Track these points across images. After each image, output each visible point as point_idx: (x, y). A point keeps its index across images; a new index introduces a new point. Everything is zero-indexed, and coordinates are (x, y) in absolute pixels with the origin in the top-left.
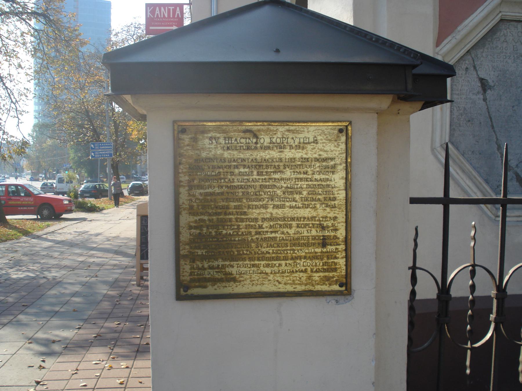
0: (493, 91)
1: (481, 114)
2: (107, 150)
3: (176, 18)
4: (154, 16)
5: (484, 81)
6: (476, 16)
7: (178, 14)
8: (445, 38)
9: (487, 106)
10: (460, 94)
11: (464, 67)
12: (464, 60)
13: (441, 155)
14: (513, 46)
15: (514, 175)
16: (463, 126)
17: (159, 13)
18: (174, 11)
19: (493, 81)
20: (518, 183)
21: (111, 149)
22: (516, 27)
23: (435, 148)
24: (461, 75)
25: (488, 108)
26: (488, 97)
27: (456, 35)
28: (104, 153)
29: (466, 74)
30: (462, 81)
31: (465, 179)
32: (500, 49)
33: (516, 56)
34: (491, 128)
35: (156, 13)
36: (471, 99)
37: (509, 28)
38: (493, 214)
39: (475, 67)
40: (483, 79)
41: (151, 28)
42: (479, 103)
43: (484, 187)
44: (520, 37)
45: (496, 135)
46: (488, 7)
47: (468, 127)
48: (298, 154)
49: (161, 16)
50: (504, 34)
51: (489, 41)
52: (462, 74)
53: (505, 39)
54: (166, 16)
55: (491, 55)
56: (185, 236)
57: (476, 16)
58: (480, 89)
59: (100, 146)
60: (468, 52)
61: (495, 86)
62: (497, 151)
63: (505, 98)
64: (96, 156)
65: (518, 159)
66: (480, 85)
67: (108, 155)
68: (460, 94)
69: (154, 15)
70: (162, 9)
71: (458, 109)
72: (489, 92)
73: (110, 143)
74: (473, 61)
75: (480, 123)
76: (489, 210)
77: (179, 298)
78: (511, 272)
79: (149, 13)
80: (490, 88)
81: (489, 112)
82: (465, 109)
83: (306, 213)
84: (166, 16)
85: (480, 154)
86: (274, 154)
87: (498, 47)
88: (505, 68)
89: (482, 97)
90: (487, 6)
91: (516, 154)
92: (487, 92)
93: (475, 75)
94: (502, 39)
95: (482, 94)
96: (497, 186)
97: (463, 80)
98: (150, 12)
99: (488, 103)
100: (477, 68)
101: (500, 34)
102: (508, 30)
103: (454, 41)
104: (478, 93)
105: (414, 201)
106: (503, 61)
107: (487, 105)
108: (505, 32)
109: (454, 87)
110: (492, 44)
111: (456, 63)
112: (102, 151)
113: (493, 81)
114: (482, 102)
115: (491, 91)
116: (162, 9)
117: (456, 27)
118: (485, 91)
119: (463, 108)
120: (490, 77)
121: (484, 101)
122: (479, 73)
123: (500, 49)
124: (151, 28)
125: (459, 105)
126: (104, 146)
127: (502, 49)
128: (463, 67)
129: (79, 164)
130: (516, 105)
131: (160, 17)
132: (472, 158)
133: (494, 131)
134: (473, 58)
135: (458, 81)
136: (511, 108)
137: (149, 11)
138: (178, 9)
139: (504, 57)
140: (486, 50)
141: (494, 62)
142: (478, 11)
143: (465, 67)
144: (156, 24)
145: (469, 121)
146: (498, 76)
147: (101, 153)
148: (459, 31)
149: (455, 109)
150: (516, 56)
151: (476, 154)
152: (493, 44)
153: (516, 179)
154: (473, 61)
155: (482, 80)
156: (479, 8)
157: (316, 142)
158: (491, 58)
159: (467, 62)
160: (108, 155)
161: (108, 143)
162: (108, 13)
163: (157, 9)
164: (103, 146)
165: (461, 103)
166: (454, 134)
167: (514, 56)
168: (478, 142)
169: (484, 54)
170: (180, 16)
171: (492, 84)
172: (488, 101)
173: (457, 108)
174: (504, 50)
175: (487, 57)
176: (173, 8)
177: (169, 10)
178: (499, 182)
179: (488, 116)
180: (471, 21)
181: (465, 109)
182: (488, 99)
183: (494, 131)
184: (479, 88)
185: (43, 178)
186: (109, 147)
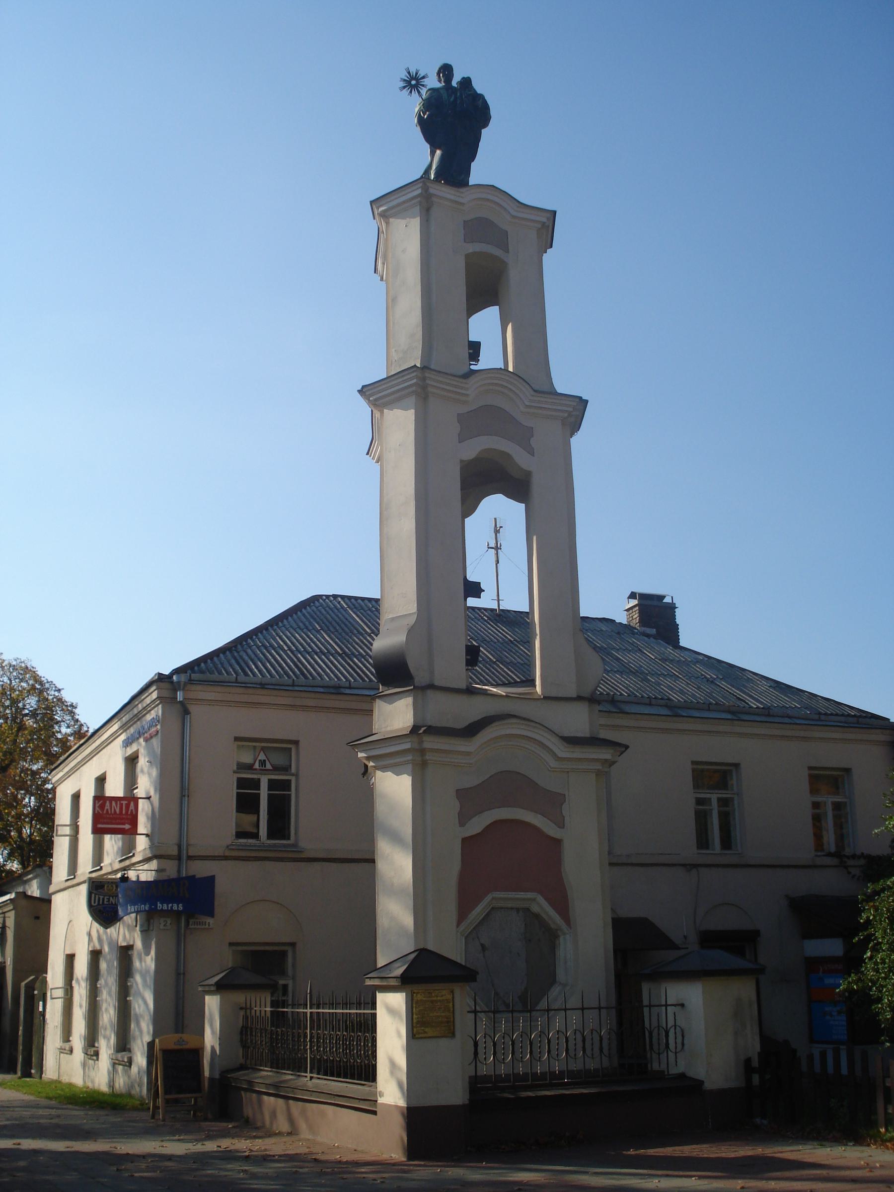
3: (129, 815)
7: (132, 810)
17: (109, 808)
18: (128, 806)
35: (106, 808)
48: (441, 999)
49: (111, 812)
56: (415, 1021)
60: (474, 928)
70: (114, 803)
78: (497, 1036)
83: (443, 1014)
84: (118, 811)
86: (435, 998)
98: (98, 807)
116: (114, 803)
124: (100, 826)
129: (417, 1000)
131: (110, 813)
137: (97, 805)
157: (445, 995)
170: (134, 813)
176: (126, 802)
185: (889, 979)
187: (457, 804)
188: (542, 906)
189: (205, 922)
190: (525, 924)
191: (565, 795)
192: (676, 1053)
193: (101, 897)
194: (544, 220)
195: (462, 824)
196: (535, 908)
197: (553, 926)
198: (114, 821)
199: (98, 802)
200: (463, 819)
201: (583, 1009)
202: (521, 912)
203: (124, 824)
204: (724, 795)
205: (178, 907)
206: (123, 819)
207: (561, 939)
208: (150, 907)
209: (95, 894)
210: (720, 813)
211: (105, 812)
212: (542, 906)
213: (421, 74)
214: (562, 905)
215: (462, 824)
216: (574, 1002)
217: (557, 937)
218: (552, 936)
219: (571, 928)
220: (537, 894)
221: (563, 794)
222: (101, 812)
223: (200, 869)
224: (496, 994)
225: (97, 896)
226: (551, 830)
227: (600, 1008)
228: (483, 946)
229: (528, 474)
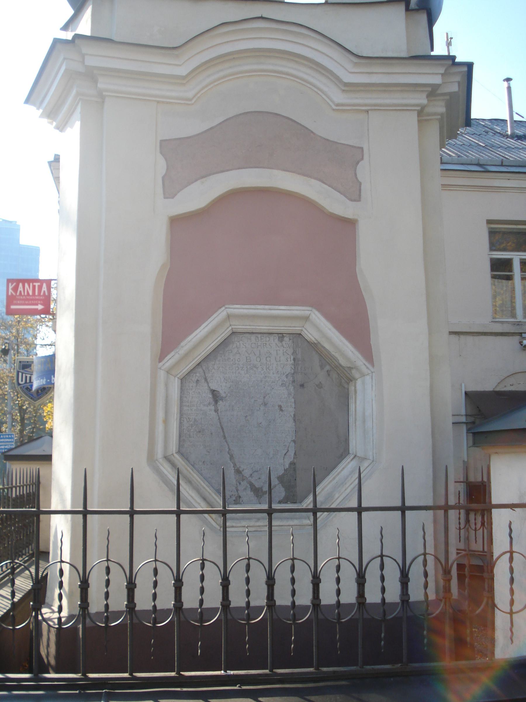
0: (224, 402)
1: (212, 425)
2: (7, 443)
5: (216, 392)
6: (200, 331)
8: (169, 353)
9: (219, 417)
10: (190, 406)
11: (194, 379)
12: (195, 373)
13: (163, 467)
14: (246, 357)
15: (248, 485)
16: (193, 437)
17: (22, 290)
18: (40, 288)
19: (225, 392)
20: (252, 493)
21: (13, 442)
22: (249, 339)
23: (157, 460)
24: (192, 388)
25: (219, 419)
26: (219, 408)
27: (179, 351)
29: (197, 386)
30: (193, 393)
31: (188, 490)
32: (232, 360)
33: (249, 367)
34: (223, 438)
35: (19, 289)
36: (201, 410)
37: (241, 340)
38: (217, 524)
39: (206, 380)
40: (214, 391)
41: (13, 307)
42: (210, 414)
43: (213, 497)
44: (253, 348)
45: (228, 445)
46: (212, 322)
47: (198, 437)
50: (237, 346)
51: (221, 354)
52: (192, 386)
53: (238, 351)
54: (31, 293)
55: (222, 367)
57: (200, 331)
58: (211, 400)
61: (227, 398)
62: (229, 461)
63: (238, 409)
65: (252, 468)
66: (211, 396)
68: (190, 406)
69: (16, 292)
70: (26, 285)
71: (188, 420)
72: (220, 403)
73: (11, 435)
74: (204, 373)
75: (211, 434)
76: (214, 520)
79: (10, 291)
80: (222, 399)
81: (220, 423)
82: (195, 420)
84: (31, 293)
85: (211, 464)
87: (230, 359)
88: (238, 379)
89: (213, 408)
90: (212, 321)
91: (250, 464)
92: (219, 403)
93: (207, 387)
95: (214, 405)
96: (230, 496)
97: (194, 392)
99: (219, 414)
100: (208, 381)
101: (232, 346)
102: (241, 342)
103: (177, 357)
104: (209, 404)
106: (236, 372)
107: (218, 415)
108: (238, 344)
109: (185, 399)
110: (224, 356)
111: (186, 376)
113: (225, 392)
114: (213, 413)
115: (223, 402)
117: (179, 343)
118: (216, 402)
119: (193, 420)
120: (222, 388)
121: (215, 412)
122: (210, 385)
123: (232, 360)
124: (13, 307)
125: (189, 417)
126: (3, 438)
127: (234, 360)
128: (193, 380)
130: (249, 415)
132: (203, 468)
133: (226, 441)
134: (204, 371)
135: (188, 394)
136: (244, 418)
138: (44, 285)
139: (237, 369)
140: (217, 362)
141: (226, 374)
142: (202, 326)
143: (196, 380)
145: (200, 432)
146: (230, 388)
148: (182, 347)
149: (185, 420)
150: (249, 367)
151: (207, 465)
152: (224, 356)
153: (250, 489)
154: (204, 373)
155: (213, 392)
156: (203, 323)
158: (223, 370)
159: (198, 374)
161: (9, 435)
162: (37, 261)
163: (21, 285)
165: (191, 415)
166: (184, 445)
167: (247, 367)
168: (209, 452)
169: (216, 367)
170: (47, 294)
171: (223, 395)
172: (219, 412)
173: (187, 420)
174: (237, 362)
175: (219, 369)
176: (39, 284)
177: (34, 287)
178: (231, 491)
179: (220, 427)
180: (195, 336)
181: (195, 420)
182: (219, 410)
183: (226, 441)
184: (210, 399)
186: (10, 440)
187: (162, 163)
190: (294, 359)
191: (362, 149)
192: (511, 613)
193: (28, 376)
196: (311, 334)
197: (343, 362)
198: (27, 302)
199: (12, 284)
201: (132, 513)
202: (286, 339)
203: (37, 304)
207: (359, 383)
208: (46, 381)
209: (22, 373)
211: (18, 293)
217: (351, 380)
219: (373, 365)
220: (309, 308)
221: (359, 148)
222: (14, 294)
224: (238, 472)
225: (24, 375)
227: (270, 512)
228: (214, 393)
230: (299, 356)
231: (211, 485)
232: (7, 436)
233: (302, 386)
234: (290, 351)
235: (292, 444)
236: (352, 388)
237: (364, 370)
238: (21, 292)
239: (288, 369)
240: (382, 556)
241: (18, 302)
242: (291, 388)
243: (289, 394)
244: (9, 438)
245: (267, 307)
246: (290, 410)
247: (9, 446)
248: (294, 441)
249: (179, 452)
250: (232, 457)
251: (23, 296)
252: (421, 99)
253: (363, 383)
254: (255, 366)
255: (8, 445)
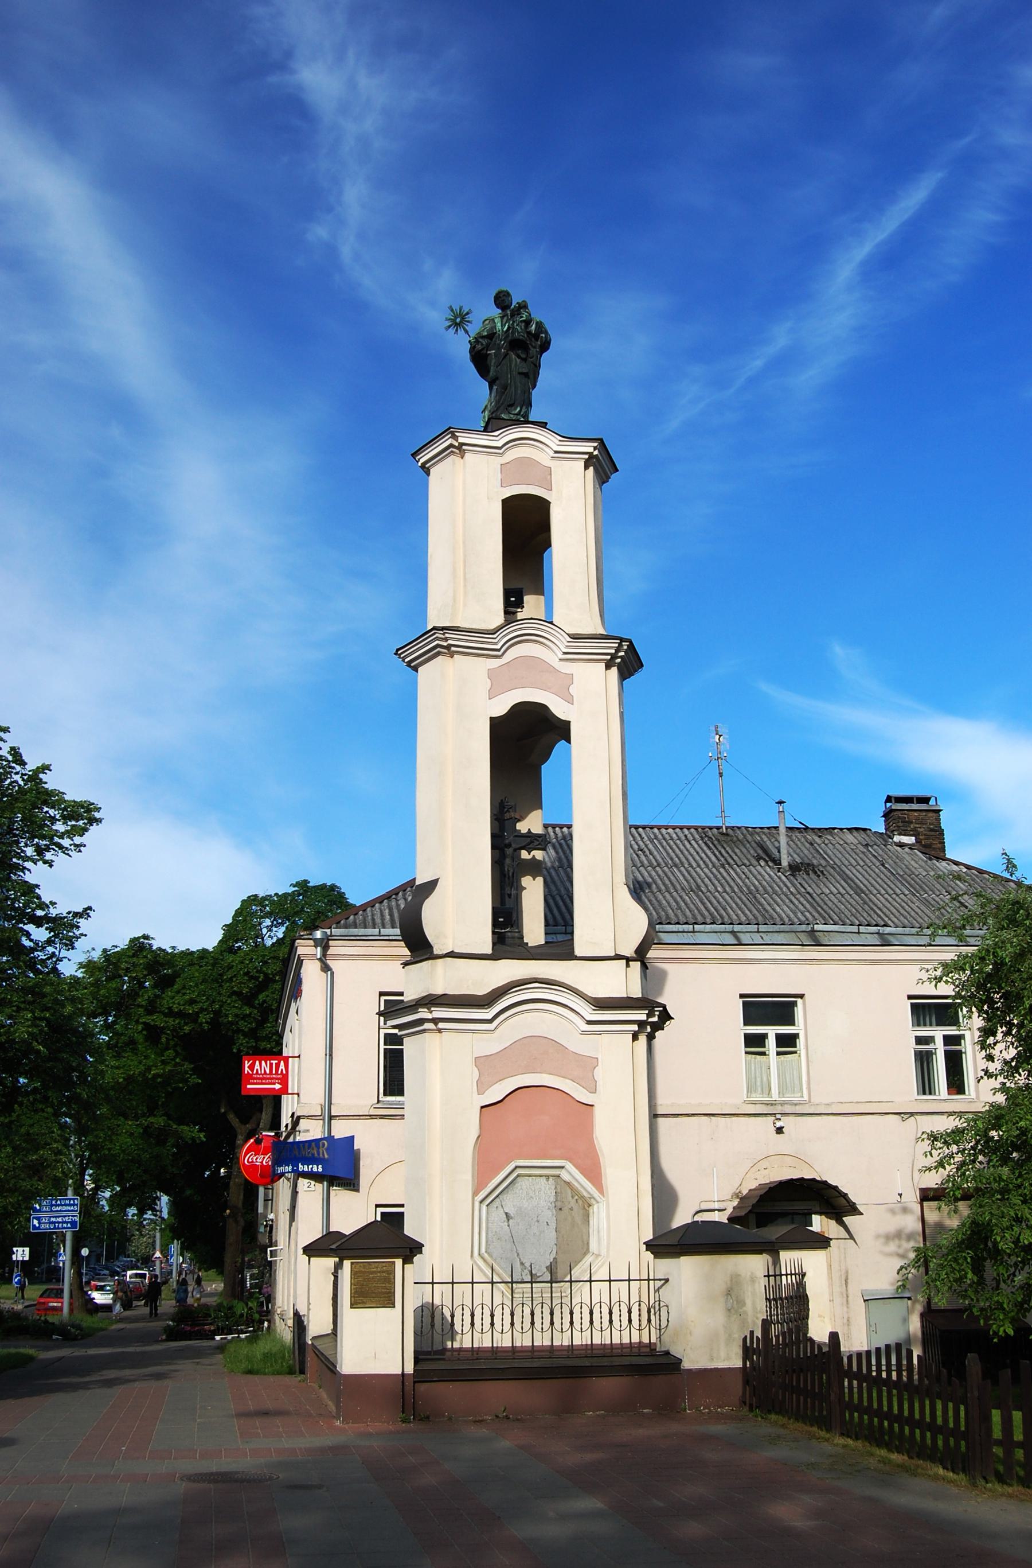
4: (253, 1071)
17: (259, 1068)
21: (77, 1211)
28: (60, 1220)
58: (506, 1219)
59: (52, 1205)
64: (43, 1227)
67: (69, 1225)
72: (511, 1221)
77: (351, 1308)
80: (512, 1218)
89: (507, 1224)
94: (520, 1187)
98: (248, 1067)
105: (415, 1283)
112: (56, 1217)
118: (508, 1220)
144: (255, 1081)
147: (54, 1220)
155: (506, 1214)
160: (69, 1225)
164: (59, 1205)
170: (284, 1072)
176: (276, 1061)
177: (271, 1064)
186: (72, 1208)
188: (571, 1173)
189: (350, 1183)
191: (597, 1058)
194: (591, 450)
195: (481, 1092)
200: (481, 1087)
201: (629, 1280)
202: (551, 1179)
203: (274, 1084)
204: (952, 1031)
205: (318, 1168)
206: (273, 1078)
207: (595, 1207)
208: (293, 1168)
210: (948, 1054)
211: (255, 1072)
212: (571, 1173)
213: (452, 331)
214: (594, 1172)
215: (481, 1092)
216: (602, 1274)
218: (586, 1204)
219: (604, 1196)
222: (251, 1073)
223: (340, 1130)
224: (522, 1264)
226: (581, 1095)
229: (568, 724)
230: (559, 1190)
231: (505, 1272)
232: (67, 1202)
233: (560, 1209)
234: (553, 1187)
235: (555, 1246)
236: (591, 1211)
237: (598, 1199)
238: (257, 1070)
239: (552, 1199)
240: (601, 1302)
241: (255, 1081)
242: (554, 1211)
243: (553, 1215)
244: (70, 1205)
245: (540, 1161)
246: (553, 1225)
247: (71, 1217)
248: (556, 1244)
249: (486, 1252)
250: (518, 1255)
251: (259, 1075)
252: (635, 1027)
253: (598, 1208)
254: (531, 1197)
255: (69, 1216)
